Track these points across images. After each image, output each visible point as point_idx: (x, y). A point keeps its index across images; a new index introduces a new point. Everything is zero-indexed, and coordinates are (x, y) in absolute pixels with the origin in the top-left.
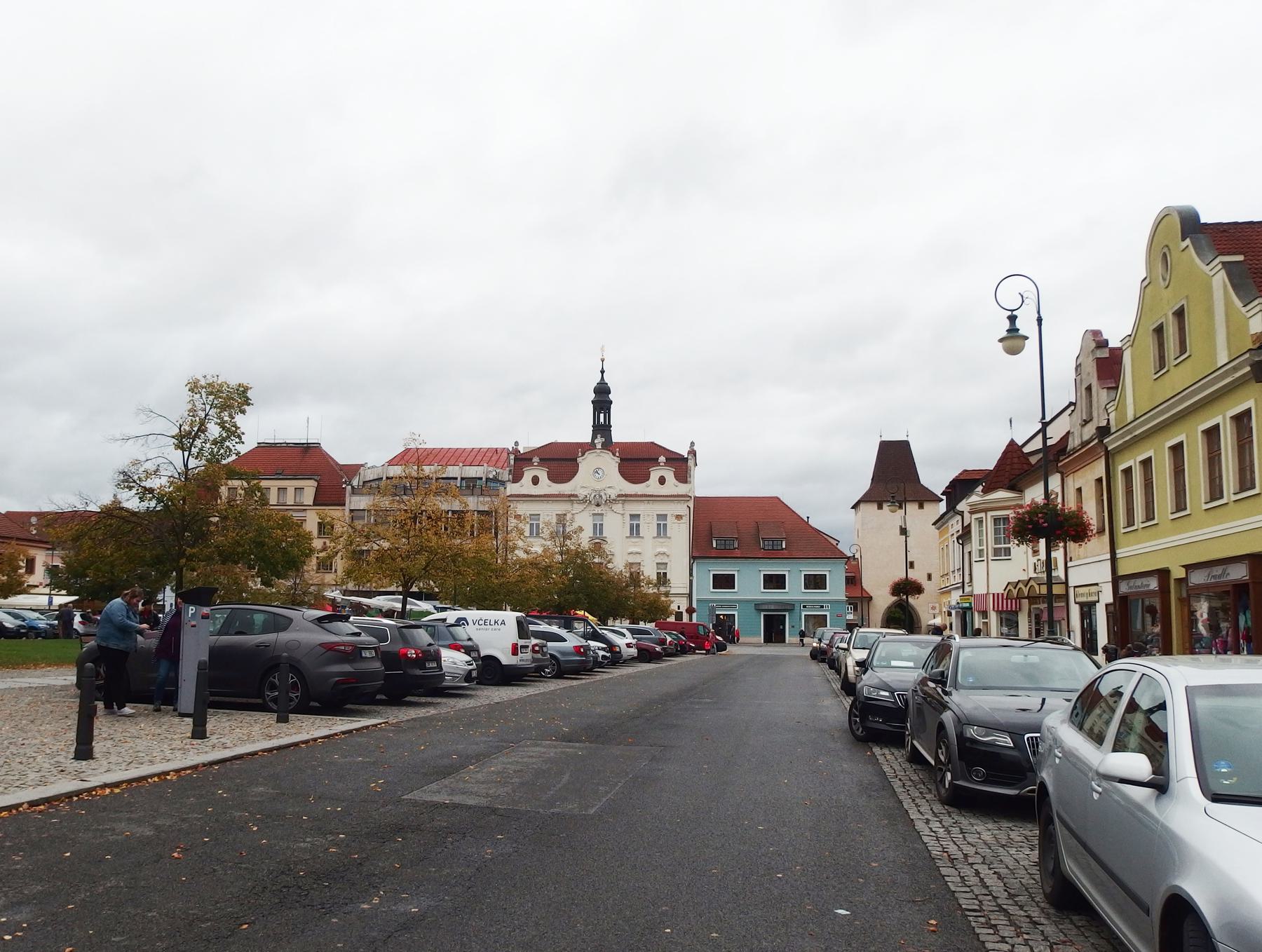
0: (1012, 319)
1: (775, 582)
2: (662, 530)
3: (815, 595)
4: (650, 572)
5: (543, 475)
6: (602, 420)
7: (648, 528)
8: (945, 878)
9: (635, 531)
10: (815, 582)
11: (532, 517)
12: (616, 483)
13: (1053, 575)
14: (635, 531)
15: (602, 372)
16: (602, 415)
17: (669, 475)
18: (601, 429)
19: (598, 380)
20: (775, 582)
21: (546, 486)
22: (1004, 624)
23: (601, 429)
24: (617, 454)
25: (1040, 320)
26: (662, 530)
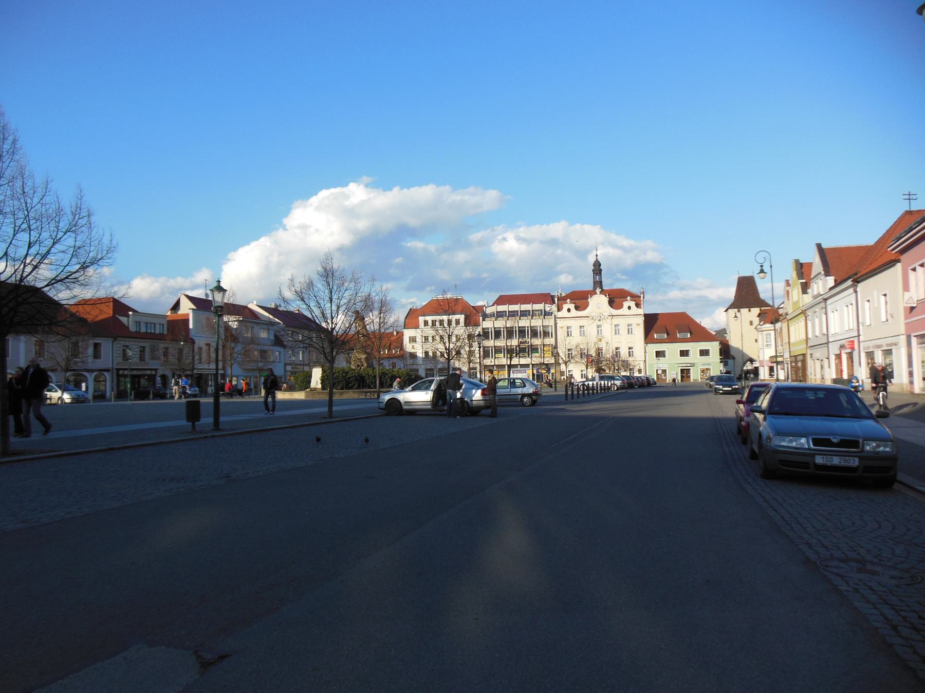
0: (762, 266)
1: (684, 353)
2: (630, 331)
3: (704, 359)
4: (624, 353)
5: (572, 306)
6: (597, 279)
7: (623, 330)
8: (872, 607)
9: (617, 332)
10: (704, 353)
11: (582, 334)
12: (607, 309)
13: (333, 410)
14: (617, 332)
15: (597, 256)
16: (597, 276)
17: (632, 304)
18: (598, 284)
19: (595, 260)
20: (684, 353)
21: (574, 312)
22: (31, 363)
23: (598, 284)
24: (607, 296)
25: (771, 266)
26: (630, 331)
